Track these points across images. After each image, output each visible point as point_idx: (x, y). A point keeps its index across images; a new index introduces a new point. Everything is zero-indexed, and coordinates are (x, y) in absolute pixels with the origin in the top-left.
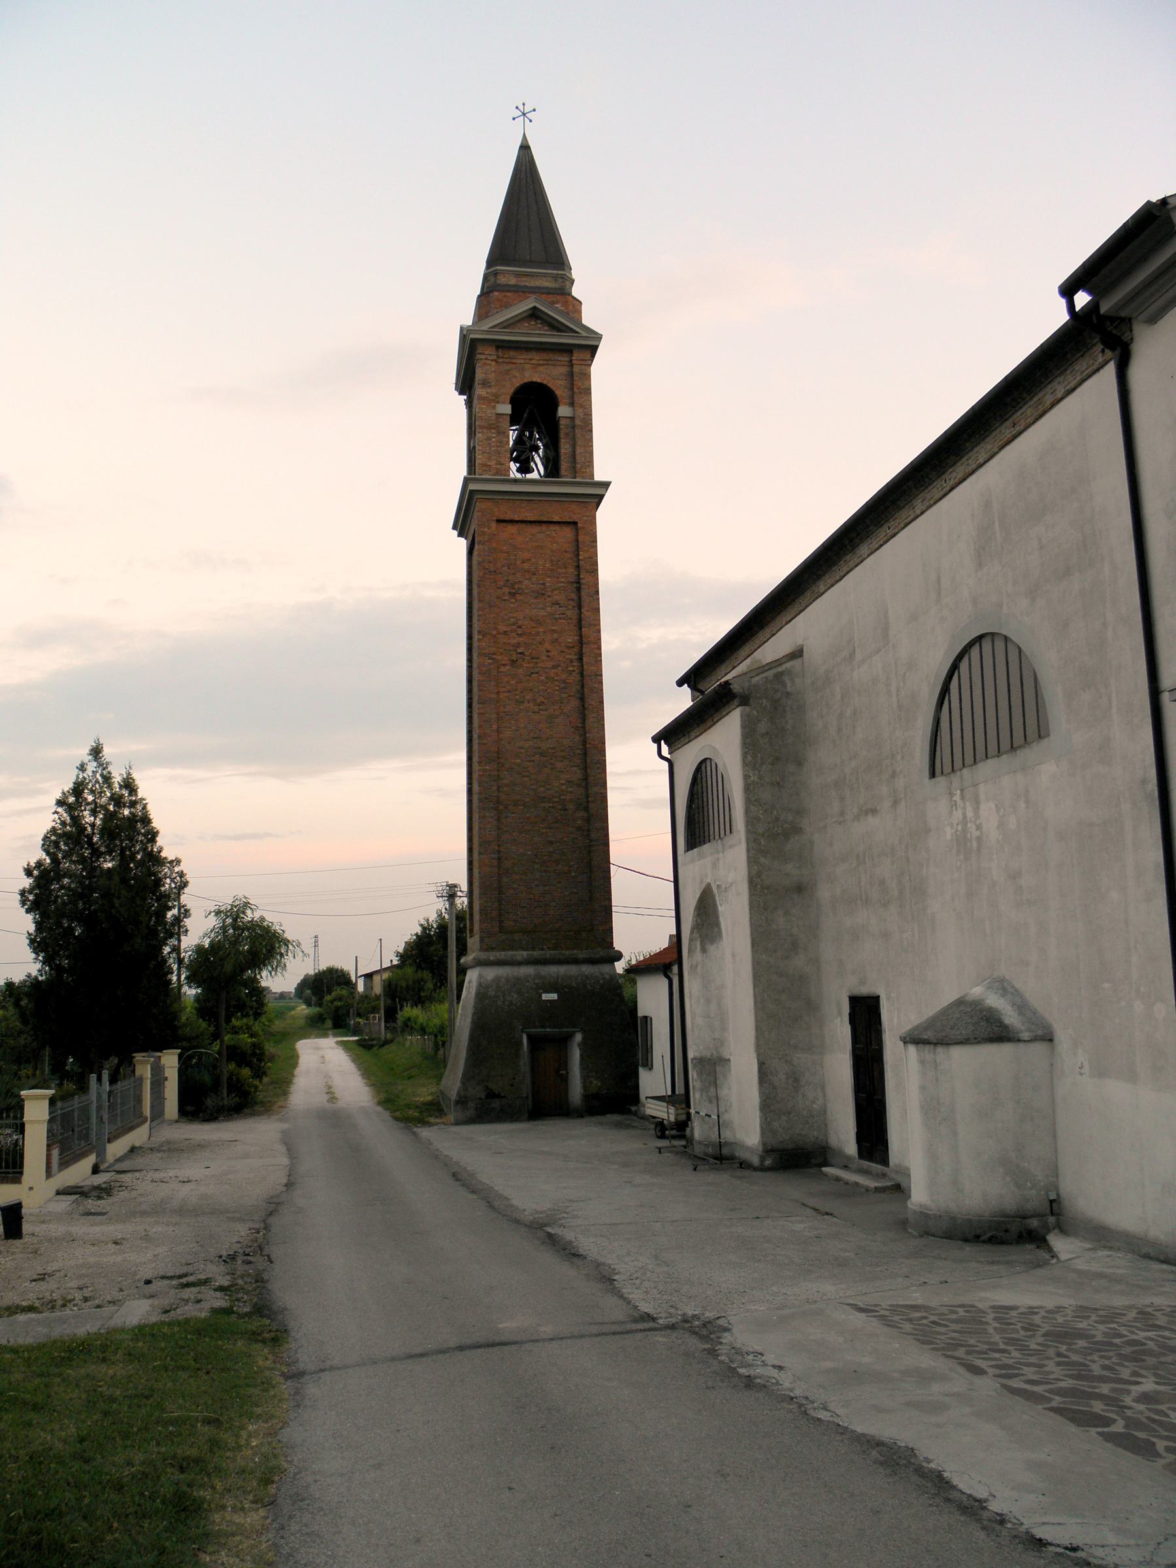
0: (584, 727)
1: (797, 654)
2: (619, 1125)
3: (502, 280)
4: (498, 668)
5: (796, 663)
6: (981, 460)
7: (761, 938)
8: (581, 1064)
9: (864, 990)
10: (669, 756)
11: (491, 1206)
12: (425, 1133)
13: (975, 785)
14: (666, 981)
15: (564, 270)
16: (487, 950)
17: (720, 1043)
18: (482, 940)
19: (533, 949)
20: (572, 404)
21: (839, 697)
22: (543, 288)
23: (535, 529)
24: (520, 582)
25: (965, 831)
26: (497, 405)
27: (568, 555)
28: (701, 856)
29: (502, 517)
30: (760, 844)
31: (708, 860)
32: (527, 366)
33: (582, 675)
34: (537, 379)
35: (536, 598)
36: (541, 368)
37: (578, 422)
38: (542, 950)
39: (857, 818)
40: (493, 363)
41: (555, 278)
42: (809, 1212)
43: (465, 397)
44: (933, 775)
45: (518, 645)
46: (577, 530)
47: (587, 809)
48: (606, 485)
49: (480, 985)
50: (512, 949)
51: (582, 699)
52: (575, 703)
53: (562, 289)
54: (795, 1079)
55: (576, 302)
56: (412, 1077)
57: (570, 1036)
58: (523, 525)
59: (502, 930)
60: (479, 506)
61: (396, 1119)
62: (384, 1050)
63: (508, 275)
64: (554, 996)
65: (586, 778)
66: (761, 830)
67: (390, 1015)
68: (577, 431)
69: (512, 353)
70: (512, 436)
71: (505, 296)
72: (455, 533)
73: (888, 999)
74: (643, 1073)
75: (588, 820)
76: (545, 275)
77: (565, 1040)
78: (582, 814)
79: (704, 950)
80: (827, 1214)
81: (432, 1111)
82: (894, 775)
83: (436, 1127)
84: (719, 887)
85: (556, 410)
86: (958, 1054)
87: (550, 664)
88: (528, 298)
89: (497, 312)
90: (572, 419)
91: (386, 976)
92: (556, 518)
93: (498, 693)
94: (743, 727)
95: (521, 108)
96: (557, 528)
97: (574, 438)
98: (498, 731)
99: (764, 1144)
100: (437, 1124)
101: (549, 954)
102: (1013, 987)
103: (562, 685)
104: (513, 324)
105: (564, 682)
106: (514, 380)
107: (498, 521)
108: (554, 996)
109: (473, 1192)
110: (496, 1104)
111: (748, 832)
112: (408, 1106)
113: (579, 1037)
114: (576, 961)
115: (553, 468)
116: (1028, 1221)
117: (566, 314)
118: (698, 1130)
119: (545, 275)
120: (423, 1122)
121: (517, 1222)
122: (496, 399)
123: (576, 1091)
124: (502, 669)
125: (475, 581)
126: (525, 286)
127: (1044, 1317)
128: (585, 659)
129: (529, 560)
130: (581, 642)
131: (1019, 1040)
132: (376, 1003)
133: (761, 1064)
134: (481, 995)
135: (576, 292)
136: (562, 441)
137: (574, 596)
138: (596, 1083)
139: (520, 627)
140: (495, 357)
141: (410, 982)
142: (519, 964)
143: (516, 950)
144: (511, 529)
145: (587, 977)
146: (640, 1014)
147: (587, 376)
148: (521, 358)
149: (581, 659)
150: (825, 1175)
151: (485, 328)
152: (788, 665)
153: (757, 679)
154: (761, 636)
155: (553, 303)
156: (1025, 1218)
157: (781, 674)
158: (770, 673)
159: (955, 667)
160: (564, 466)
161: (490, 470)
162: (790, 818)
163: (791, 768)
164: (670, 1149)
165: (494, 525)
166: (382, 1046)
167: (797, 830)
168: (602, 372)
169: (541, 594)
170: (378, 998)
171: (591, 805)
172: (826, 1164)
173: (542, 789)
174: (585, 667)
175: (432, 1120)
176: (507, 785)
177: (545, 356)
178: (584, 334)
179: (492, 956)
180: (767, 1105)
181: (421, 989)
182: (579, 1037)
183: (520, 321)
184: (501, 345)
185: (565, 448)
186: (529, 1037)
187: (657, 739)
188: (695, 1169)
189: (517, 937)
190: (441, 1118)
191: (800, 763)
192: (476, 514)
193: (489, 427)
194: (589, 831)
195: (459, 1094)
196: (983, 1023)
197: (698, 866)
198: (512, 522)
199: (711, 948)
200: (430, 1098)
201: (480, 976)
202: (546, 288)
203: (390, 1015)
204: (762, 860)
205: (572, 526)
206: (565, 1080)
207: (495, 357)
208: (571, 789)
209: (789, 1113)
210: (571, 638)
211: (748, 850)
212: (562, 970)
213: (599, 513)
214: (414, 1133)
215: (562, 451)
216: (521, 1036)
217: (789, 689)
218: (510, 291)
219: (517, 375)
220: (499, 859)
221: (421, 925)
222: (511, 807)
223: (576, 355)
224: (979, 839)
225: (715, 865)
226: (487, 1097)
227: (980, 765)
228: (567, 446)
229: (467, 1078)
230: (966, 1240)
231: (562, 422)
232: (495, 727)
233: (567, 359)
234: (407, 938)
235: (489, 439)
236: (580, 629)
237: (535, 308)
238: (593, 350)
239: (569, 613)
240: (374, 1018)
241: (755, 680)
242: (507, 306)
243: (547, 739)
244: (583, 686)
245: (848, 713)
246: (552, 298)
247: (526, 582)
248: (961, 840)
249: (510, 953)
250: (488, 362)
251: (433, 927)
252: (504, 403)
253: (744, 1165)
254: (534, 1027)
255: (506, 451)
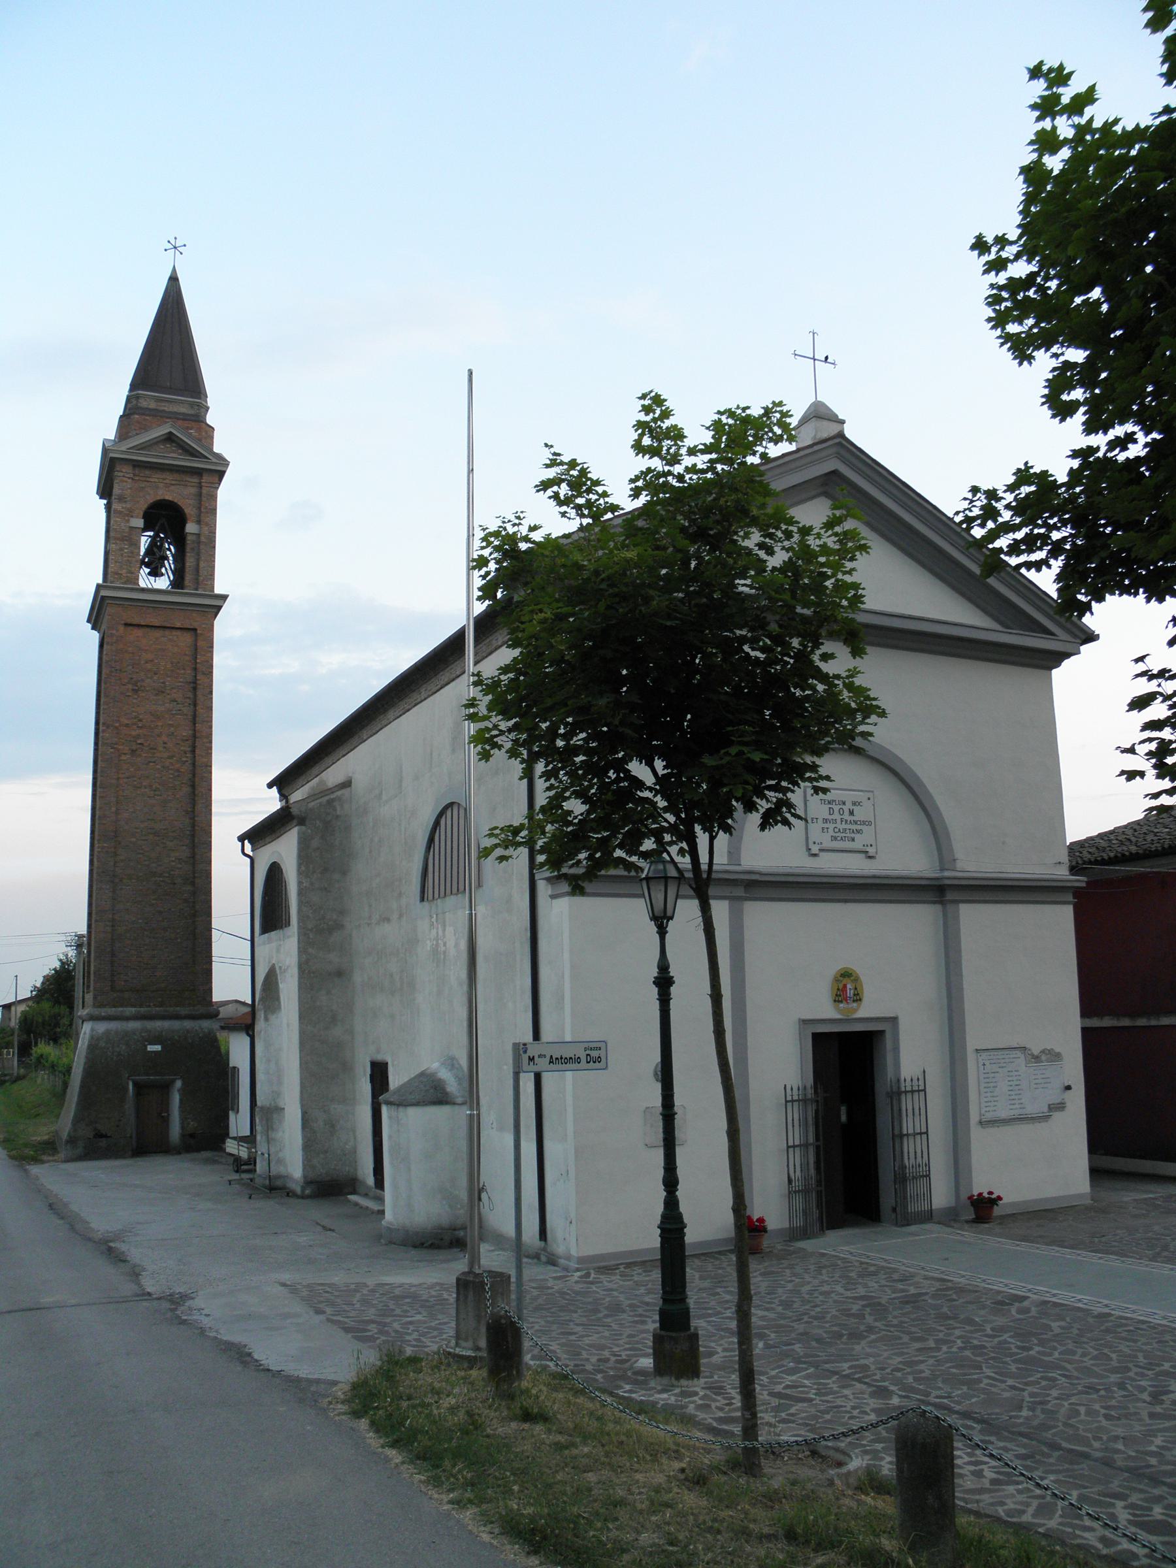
0: (193, 812)
1: (347, 784)
2: (207, 1161)
3: (144, 403)
4: (120, 756)
5: (345, 792)
6: (458, 673)
7: (307, 1013)
8: (180, 1107)
9: (379, 1057)
10: (251, 854)
11: (72, 1228)
12: (35, 1170)
13: (444, 913)
14: (247, 1040)
15: (200, 398)
16: (99, 1007)
17: (277, 1094)
18: (95, 998)
19: (141, 1006)
20: (199, 522)
21: (371, 824)
22: (180, 414)
23: (158, 633)
24: (143, 680)
25: (437, 945)
26: (131, 519)
27: (187, 658)
28: (270, 941)
29: (129, 621)
30: (309, 938)
31: (274, 945)
32: (161, 485)
33: (194, 764)
34: (168, 497)
35: (157, 695)
36: (172, 488)
37: (203, 539)
38: (149, 1006)
39: (378, 923)
40: (130, 481)
41: (192, 405)
42: (319, 1229)
43: (105, 501)
44: (422, 899)
45: (138, 736)
46: (196, 635)
47: (193, 884)
48: (224, 598)
49: (92, 1037)
50: (122, 1006)
51: (193, 786)
52: (186, 790)
53: (196, 418)
54: (332, 1126)
55: (208, 428)
56: (38, 1115)
57: (173, 1081)
58: (148, 630)
59: (113, 989)
60: (109, 610)
61: (12, 1157)
62: (15, 1087)
63: (150, 398)
64: (158, 1048)
65: (193, 856)
66: (310, 927)
67: (24, 1050)
68: (202, 547)
69: (147, 472)
70: (144, 542)
71: (145, 420)
72: (90, 626)
73: (393, 1065)
74: (232, 1115)
75: (194, 893)
76: (182, 402)
77: (166, 1087)
78: (189, 888)
79: (266, 1019)
80: (330, 1230)
81: (47, 1149)
82: (400, 895)
83: (47, 1165)
84: (280, 967)
85: (185, 526)
86: (412, 1112)
87: (166, 755)
88: (166, 422)
89: (137, 434)
90: (198, 535)
91: (22, 1008)
92: (178, 625)
93: (118, 779)
94: (300, 843)
95: (173, 242)
96: (179, 633)
97: (198, 554)
98: (117, 813)
99: (305, 1177)
100: (48, 1161)
101: (155, 1010)
102: (459, 1064)
103: (176, 774)
104: (151, 445)
105: (178, 771)
106: (148, 497)
107: (126, 624)
108: (158, 1048)
109: (62, 1218)
110: (103, 1143)
111: (299, 927)
112: (26, 1145)
113: (179, 1084)
114: (177, 1017)
115: (178, 582)
116: (457, 1232)
117: (199, 440)
118: (260, 1167)
119: (182, 402)
120: (36, 1160)
121: (90, 1239)
122: (130, 514)
123: (175, 1131)
124: (123, 757)
125: (103, 676)
126: (164, 411)
127: (621, 1335)
128: (198, 752)
129: (152, 661)
130: (194, 736)
131: (454, 1104)
132: (11, 1038)
133: (304, 1114)
134: (92, 1047)
135: (210, 419)
136: (188, 554)
137: (190, 695)
138: (192, 1124)
139: (140, 720)
140: (132, 475)
141: (47, 1018)
142: (128, 1019)
143: (126, 1006)
144: (139, 632)
145: (188, 1031)
146: (231, 1065)
147: (213, 498)
148: (156, 477)
149: (193, 751)
150: (349, 1201)
151: (124, 449)
152: (339, 793)
153: (313, 804)
154: (328, 760)
155: (188, 428)
156: (455, 1230)
157: (333, 800)
158: (324, 799)
159: (437, 824)
160: (188, 578)
161: (121, 578)
162: (335, 917)
163: (336, 876)
164: (239, 1181)
165: (122, 628)
166: (15, 1081)
167: (339, 926)
168: (226, 493)
169: (160, 692)
170: (13, 1031)
171: (197, 881)
172: (354, 1192)
173: (154, 865)
174: (197, 758)
175: (45, 1158)
176: (122, 861)
177: (177, 476)
178: (214, 460)
179: (104, 1012)
180: (308, 1146)
181: (57, 1025)
182: (179, 1084)
183: (156, 443)
184: (136, 465)
185: (190, 561)
186: (135, 1084)
187: (241, 839)
188: (250, 1198)
189: (126, 995)
190: (53, 1155)
191: (344, 873)
192: (106, 618)
193: (122, 539)
194: (194, 902)
195: (69, 1135)
196: (432, 1091)
197: (268, 946)
198: (139, 626)
199: (272, 1018)
200: (46, 1137)
201: (92, 1030)
202: (183, 414)
203: (24, 1050)
204: (310, 950)
205: (192, 633)
206: (166, 1121)
207: (132, 475)
208: (180, 866)
209: (326, 1152)
210: (186, 732)
211: (299, 942)
212: (166, 1024)
213: (216, 622)
214: (25, 1170)
215: (188, 564)
216: (128, 1084)
217: (338, 813)
218: (149, 415)
219: (151, 492)
220: (113, 926)
221: (60, 960)
222: (125, 881)
223: (206, 478)
224: (445, 952)
225: (278, 951)
226: (94, 1137)
227: (447, 898)
228: (192, 560)
229: (77, 1121)
230: (415, 1247)
231: (189, 538)
232: (114, 809)
233: (196, 480)
234: (46, 972)
235: (121, 549)
236: (195, 724)
237: (170, 433)
238: (221, 474)
239: (185, 710)
240: (8, 1053)
241: (311, 805)
242: (145, 428)
243: (161, 821)
244: (194, 775)
245: (376, 839)
246: (186, 424)
247: (148, 680)
248: (435, 951)
249: (121, 1009)
250: (125, 479)
251: (71, 962)
252: (137, 517)
253: (290, 1194)
254: (139, 1075)
255: (137, 561)
